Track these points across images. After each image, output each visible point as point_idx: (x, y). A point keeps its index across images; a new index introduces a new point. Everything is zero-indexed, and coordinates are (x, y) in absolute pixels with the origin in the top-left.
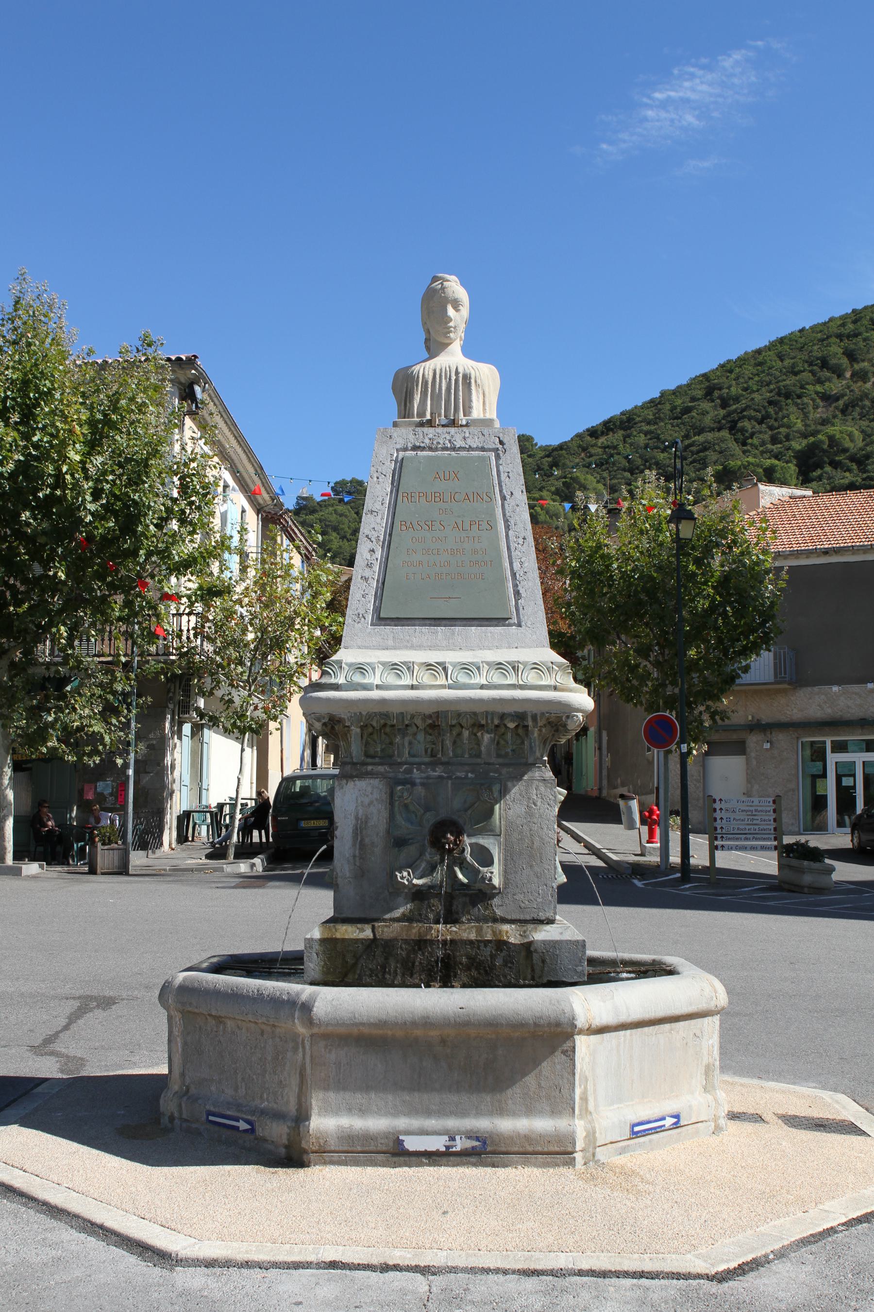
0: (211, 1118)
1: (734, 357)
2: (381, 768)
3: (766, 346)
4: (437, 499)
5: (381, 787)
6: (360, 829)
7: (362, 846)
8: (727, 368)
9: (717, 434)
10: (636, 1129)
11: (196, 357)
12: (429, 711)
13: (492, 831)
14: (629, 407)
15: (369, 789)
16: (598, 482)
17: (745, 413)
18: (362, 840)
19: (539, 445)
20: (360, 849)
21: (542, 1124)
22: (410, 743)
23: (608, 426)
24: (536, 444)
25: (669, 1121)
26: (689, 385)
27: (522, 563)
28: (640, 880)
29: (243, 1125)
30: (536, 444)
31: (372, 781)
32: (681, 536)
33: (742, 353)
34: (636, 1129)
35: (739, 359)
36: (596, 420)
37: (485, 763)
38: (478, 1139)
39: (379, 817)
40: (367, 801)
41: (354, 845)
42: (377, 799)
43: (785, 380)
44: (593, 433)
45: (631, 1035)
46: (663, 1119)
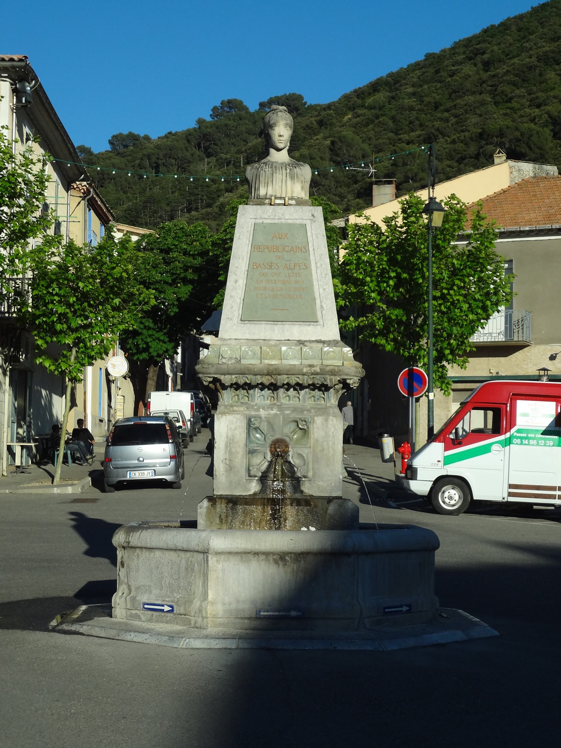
0: (146, 606)
1: (497, 23)
2: (242, 409)
3: (528, 12)
4: (275, 250)
5: (241, 419)
6: (230, 443)
7: (230, 453)
8: (489, 33)
9: (479, 97)
10: (386, 610)
11: (26, 57)
14: (395, 69)
15: (235, 420)
16: (364, 141)
17: (505, 78)
19: (308, 104)
20: (229, 455)
23: (375, 87)
24: (305, 103)
25: (405, 609)
26: (452, 48)
28: (394, 502)
29: (166, 608)
30: (305, 103)
31: (236, 416)
32: (433, 225)
33: (505, 18)
35: (502, 24)
36: (363, 80)
39: (241, 434)
40: (233, 427)
41: (226, 452)
42: (239, 426)
43: (544, 47)
44: (360, 93)
46: (401, 606)
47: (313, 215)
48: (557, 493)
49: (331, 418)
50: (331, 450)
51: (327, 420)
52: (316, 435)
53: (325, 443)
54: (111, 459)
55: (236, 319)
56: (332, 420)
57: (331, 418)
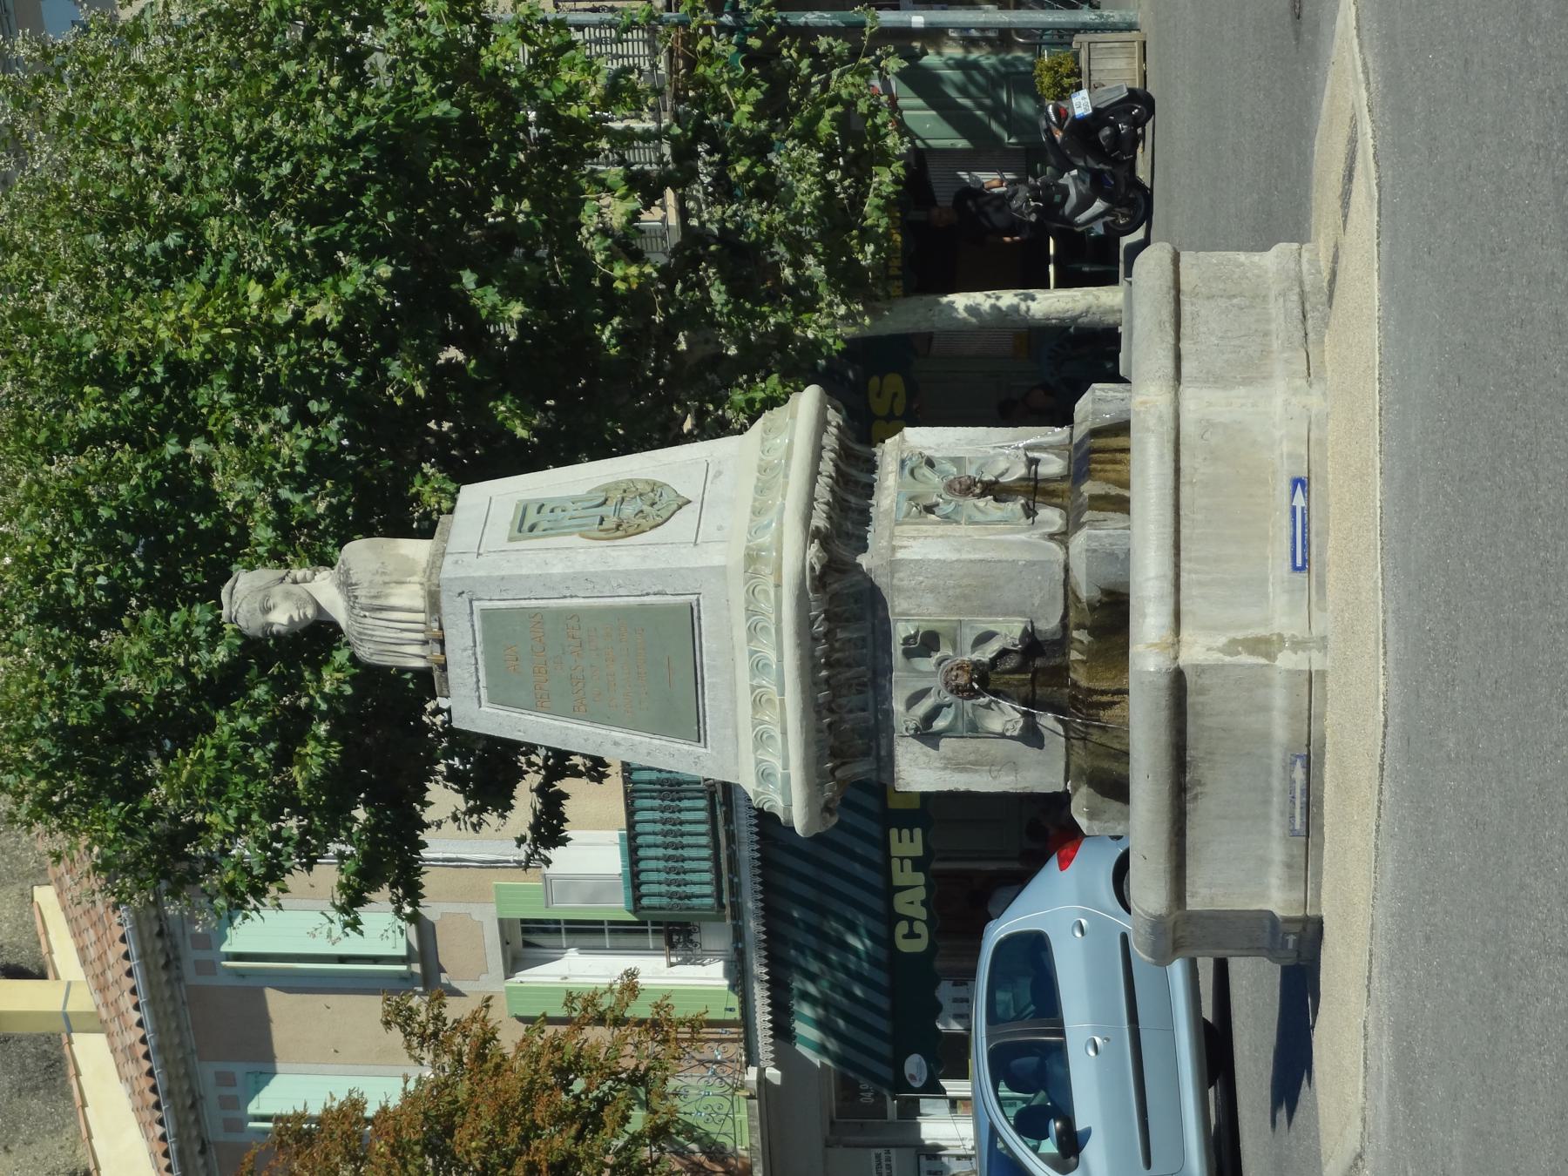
10: (1299, 563)
12: (813, 716)
13: (955, 629)
18: (970, 763)
21: (1279, 699)
22: (851, 711)
25: (1299, 501)
27: (619, 586)
34: (1299, 563)
37: (873, 632)
38: (1293, 763)
41: (976, 771)
45: (1190, 560)
46: (1294, 509)
47: (460, 594)
48: (884, 1171)
49: (895, 581)
50: (965, 582)
51: (900, 590)
52: (932, 609)
53: (951, 593)
54: (1112, 144)
55: (698, 750)
56: (901, 580)
57: (895, 581)
